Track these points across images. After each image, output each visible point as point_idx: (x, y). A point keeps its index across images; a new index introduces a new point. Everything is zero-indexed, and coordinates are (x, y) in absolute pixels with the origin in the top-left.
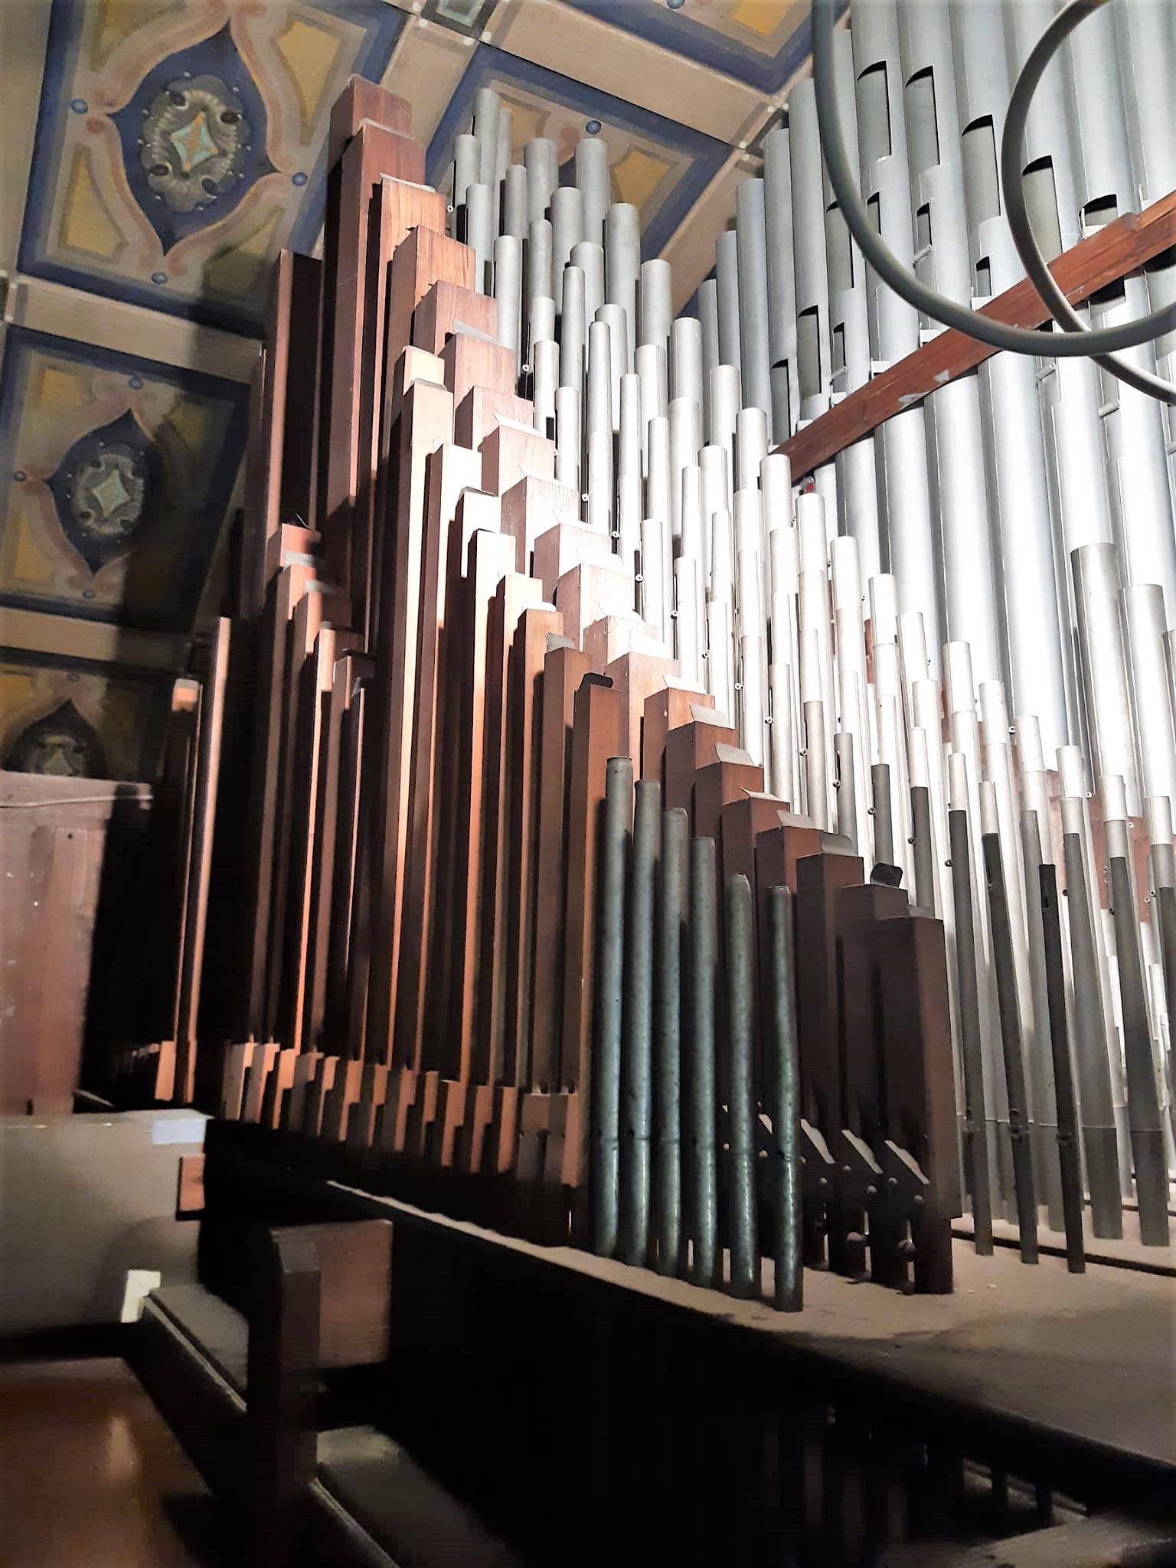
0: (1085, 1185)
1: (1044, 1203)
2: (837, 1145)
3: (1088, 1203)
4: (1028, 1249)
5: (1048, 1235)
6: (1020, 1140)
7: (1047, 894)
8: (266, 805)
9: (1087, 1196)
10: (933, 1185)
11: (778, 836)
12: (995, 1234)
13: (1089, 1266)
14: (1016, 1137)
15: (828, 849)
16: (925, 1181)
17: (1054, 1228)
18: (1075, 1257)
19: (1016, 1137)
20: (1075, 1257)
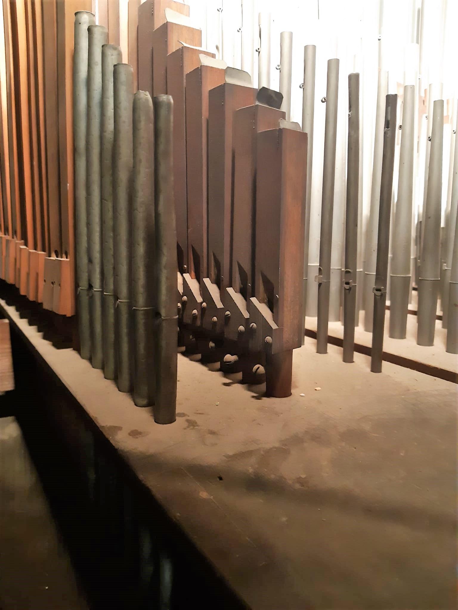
0: (388, 296)
1: (364, 309)
2: (225, 297)
3: (388, 308)
4: (348, 346)
5: (363, 336)
6: (350, 289)
7: (389, 118)
8: (68, 135)
9: (388, 303)
10: (280, 330)
11: (199, 72)
12: (330, 334)
13: (386, 365)
14: (347, 287)
15: (229, 80)
16: (274, 326)
17: (367, 330)
18: (377, 355)
19: (347, 287)
20: (377, 355)
